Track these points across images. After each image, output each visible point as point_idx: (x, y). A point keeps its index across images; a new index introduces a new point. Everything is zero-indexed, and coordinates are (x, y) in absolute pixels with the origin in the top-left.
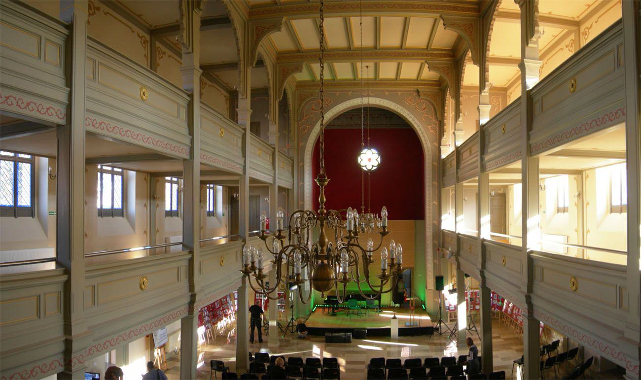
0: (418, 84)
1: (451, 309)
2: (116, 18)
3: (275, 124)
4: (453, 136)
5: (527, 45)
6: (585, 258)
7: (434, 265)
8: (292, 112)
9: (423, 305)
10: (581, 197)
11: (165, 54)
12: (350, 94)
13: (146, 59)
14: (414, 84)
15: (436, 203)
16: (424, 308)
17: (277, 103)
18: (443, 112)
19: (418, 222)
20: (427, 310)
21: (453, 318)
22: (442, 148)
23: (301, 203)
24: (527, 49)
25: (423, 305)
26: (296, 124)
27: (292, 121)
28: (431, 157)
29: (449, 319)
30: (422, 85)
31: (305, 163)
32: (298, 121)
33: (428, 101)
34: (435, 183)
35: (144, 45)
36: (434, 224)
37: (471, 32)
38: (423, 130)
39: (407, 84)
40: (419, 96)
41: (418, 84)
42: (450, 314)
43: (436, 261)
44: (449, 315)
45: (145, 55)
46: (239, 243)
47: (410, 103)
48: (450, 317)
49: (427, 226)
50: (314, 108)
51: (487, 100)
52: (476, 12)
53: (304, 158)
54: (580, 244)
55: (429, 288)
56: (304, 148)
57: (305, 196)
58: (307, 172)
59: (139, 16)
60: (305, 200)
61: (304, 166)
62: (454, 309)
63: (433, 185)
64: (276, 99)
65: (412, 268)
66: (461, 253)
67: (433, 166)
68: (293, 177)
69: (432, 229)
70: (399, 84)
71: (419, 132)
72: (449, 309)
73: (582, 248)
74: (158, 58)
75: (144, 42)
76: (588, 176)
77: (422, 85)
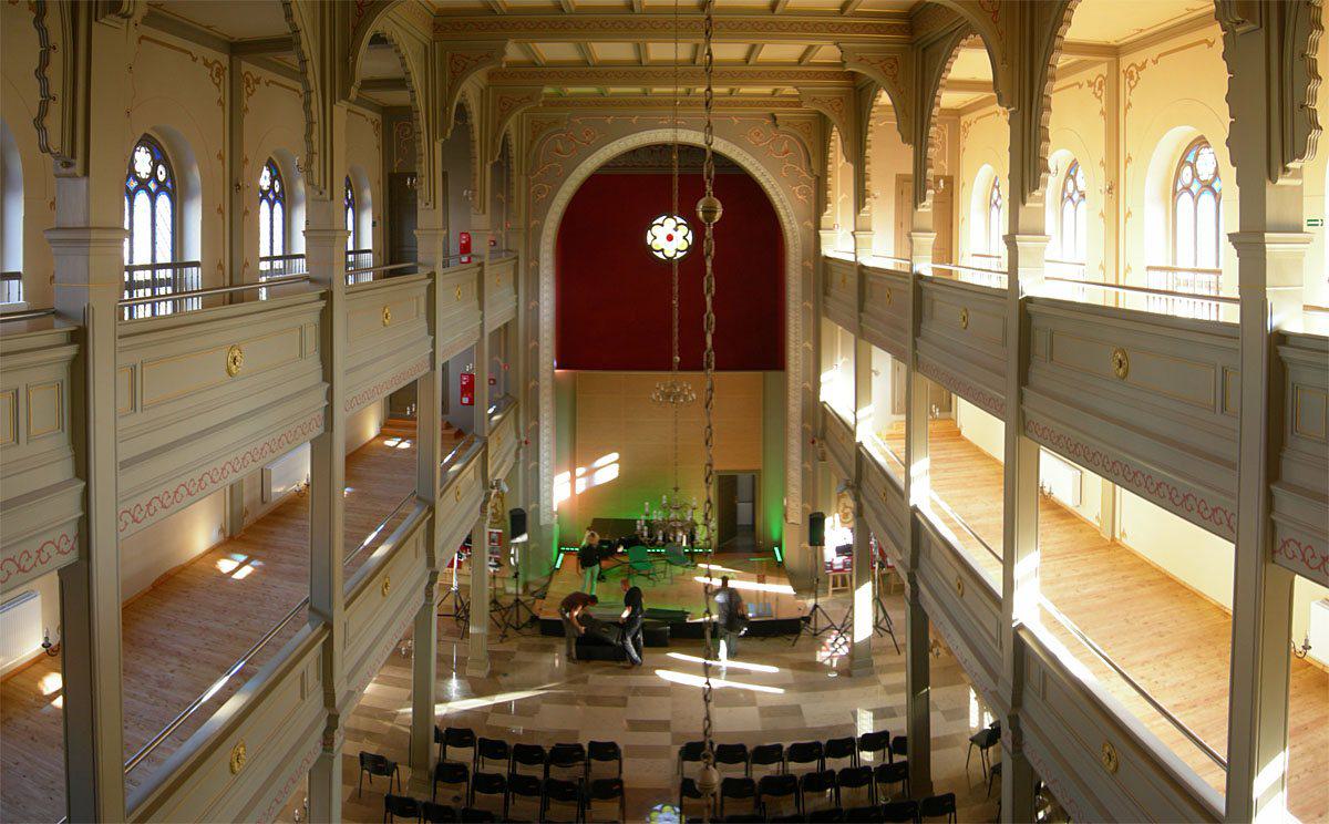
0: (772, 104)
1: (835, 568)
2: (163, 44)
3: (484, 213)
4: (852, 238)
5: (1024, 203)
6: (1121, 306)
7: (804, 472)
8: (515, 160)
9: (776, 549)
10: (1114, 197)
11: (258, 83)
12: (634, 121)
13: (221, 162)
14: (767, 104)
15: (810, 346)
16: (779, 559)
17: (488, 167)
18: (824, 161)
19: (771, 374)
20: (787, 564)
21: (839, 587)
22: (822, 233)
23: (533, 304)
24: (1022, 210)
25: (776, 549)
26: (523, 178)
27: (514, 179)
28: (799, 251)
29: (831, 589)
30: (781, 104)
31: (541, 261)
32: (527, 175)
33: (795, 136)
34: (808, 345)
35: (217, 80)
36: (805, 389)
37: (895, 76)
38: (783, 196)
39: (751, 104)
40: (777, 126)
41: (772, 104)
42: (834, 577)
43: (807, 425)
44: (831, 580)
45: (219, 209)
46: (415, 286)
47: (758, 140)
48: (833, 586)
49: (792, 385)
50: (561, 147)
51: (929, 222)
52: (904, 33)
53: (538, 400)
54: (1108, 282)
55: (791, 520)
56: (539, 231)
57: (541, 321)
58: (546, 423)
59: (208, 27)
60: (541, 339)
61: (538, 267)
62: (841, 567)
63: (805, 309)
64: (486, 162)
65: (758, 471)
66: (865, 485)
67: (805, 269)
68: (517, 292)
69: (800, 399)
70: (736, 104)
71: (776, 199)
72: (831, 568)
73: (1115, 289)
74: (246, 94)
75: (218, 75)
76: (1130, 104)
77: (781, 104)
